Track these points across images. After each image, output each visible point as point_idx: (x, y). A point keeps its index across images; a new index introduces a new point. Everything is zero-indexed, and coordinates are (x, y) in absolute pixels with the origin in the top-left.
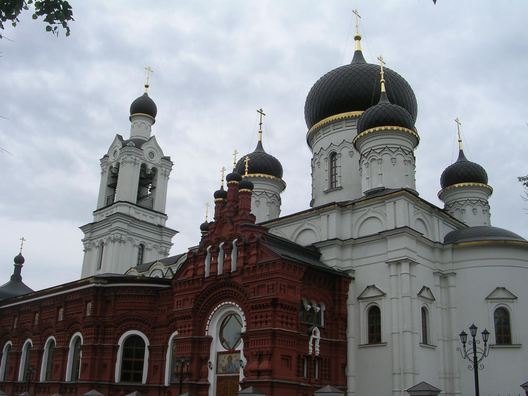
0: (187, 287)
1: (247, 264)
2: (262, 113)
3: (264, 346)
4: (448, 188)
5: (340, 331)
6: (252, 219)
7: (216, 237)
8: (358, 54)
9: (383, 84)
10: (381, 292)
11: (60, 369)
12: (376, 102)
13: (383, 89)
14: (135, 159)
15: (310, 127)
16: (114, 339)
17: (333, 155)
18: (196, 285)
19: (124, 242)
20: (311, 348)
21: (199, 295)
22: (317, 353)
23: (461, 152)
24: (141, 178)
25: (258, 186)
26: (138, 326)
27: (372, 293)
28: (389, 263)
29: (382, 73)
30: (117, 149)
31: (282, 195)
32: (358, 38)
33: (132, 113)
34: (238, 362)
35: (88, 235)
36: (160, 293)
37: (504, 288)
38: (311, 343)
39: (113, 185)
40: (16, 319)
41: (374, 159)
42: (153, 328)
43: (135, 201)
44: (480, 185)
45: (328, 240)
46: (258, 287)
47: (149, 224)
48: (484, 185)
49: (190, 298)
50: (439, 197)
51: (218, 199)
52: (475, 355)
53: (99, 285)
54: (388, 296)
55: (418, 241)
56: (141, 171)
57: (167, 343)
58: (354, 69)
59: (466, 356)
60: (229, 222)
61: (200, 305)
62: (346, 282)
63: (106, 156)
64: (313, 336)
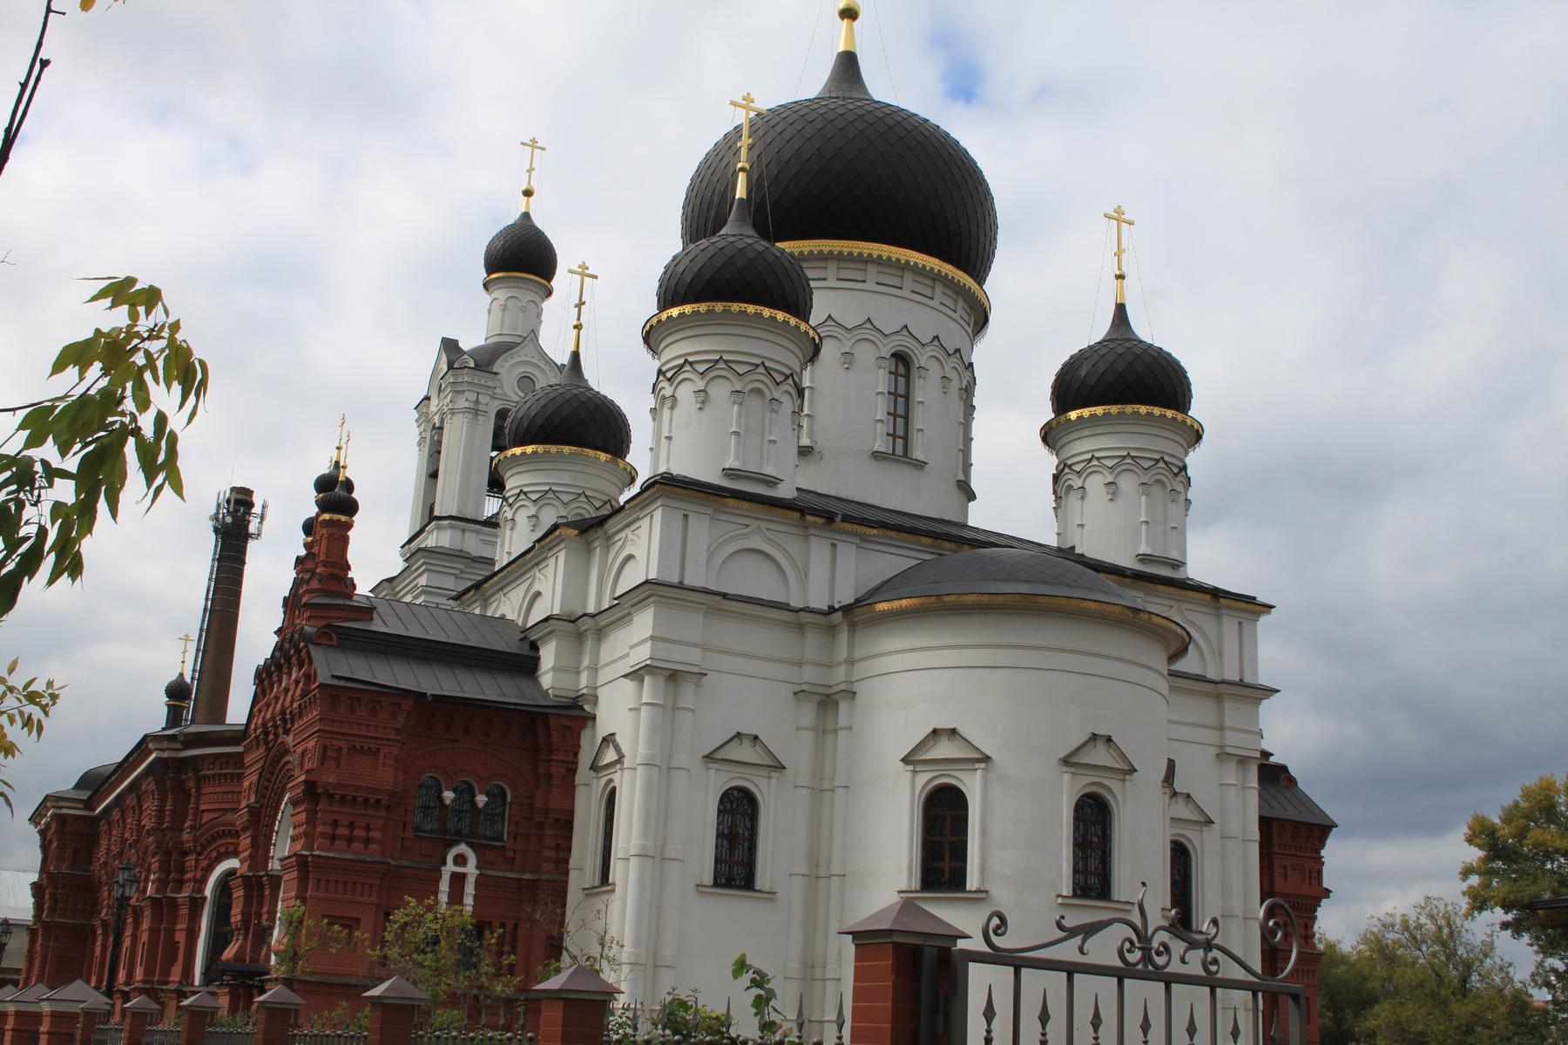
2: (583, 275)
9: (742, 178)
13: (740, 192)
14: (477, 402)
16: (196, 881)
33: (490, 271)
37: (756, 738)
44: (1169, 413)
48: (1180, 417)
53: (166, 755)
55: (711, 611)
58: (831, 116)
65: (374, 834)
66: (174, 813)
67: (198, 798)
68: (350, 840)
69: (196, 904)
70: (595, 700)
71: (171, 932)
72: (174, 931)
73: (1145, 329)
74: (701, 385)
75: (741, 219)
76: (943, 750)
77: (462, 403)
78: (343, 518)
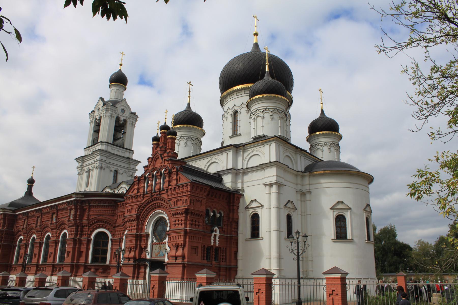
0: (134, 200)
1: (170, 185)
2: (190, 84)
3: (180, 240)
4: (312, 135)
5: (233, 230)
6: (175, 156)
7: (152, 167)
8: (256, 45)
9: (267, 67)
10: (260, 204)
11: (53, 255)
12: (262, 77)
13: (267, 69)
14: (112, 114)
15: (222, 93)
16: (88, 234)
17: (236, 113)
19: (104, 169)
20: (212, 241)
22: (217, 244)
23: (322, 111)
24: (116, 126)
25: (179, 133)
26: (101, 226)
28: (266, 185)
29: (267, 58)
30: (100, 107)
31: (203, 139)
32: (256, 34)
33: (110, 83)
34: (164, 251)
35: (81, 164)
36: (119, 204)
39: (97, 131)
40: (26, 222)
41: (259, 116)
42: (114, 227)
43: (111, 141)
44: (334, 133)
45: (227, 170)
46: (177, 201)
47: (121, 156)
48: (336, 133)
49: (135, 207)
50: (307, 140)
51: (154, 142)
52: (298, 250)
53: (79, 199)
55: (285, 170)
58: (255, 55)
59: (293, 251)
60: (160, 157)
61: (141, 212)
62: (238, 197)
63: (93, 112)
64: (214, 233)
65: (200, 224)
66: (80, 215)
67: (89, 211)
68: (195, 225)
69: (89, 241)
70: (243, 191)
71: (79, 248)
72: (80, 248)
73: (328, 114)
74: (271, 114)
75: (268, 76)
76: (340, 206)
77: (108, 114)
78: (174, 137)
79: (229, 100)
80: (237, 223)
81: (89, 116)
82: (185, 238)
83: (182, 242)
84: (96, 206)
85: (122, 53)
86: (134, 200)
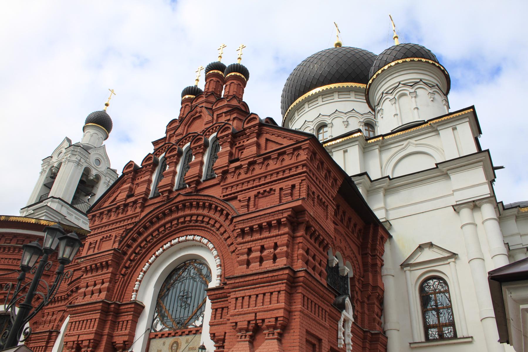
10: (450, 252)
14: (80, 160)
18: (130, 212)
21: (131, 229)
24: (81, 182)
27: (427, 255)
28: (457, 208)
38: (341, 324)
39: (48, 186)
43: (70, 203)
46: (256, 196)
54: (463, 258)
56: (83, 175)
57: (59, 327)
77: (74, 158)
79: (307, 110)
80: (381, 301)
81: (42, 162)
82: (290, 300)
83: (281, 313)
84: (9, 248)
85: (112, 91)
86: (113, 218)
